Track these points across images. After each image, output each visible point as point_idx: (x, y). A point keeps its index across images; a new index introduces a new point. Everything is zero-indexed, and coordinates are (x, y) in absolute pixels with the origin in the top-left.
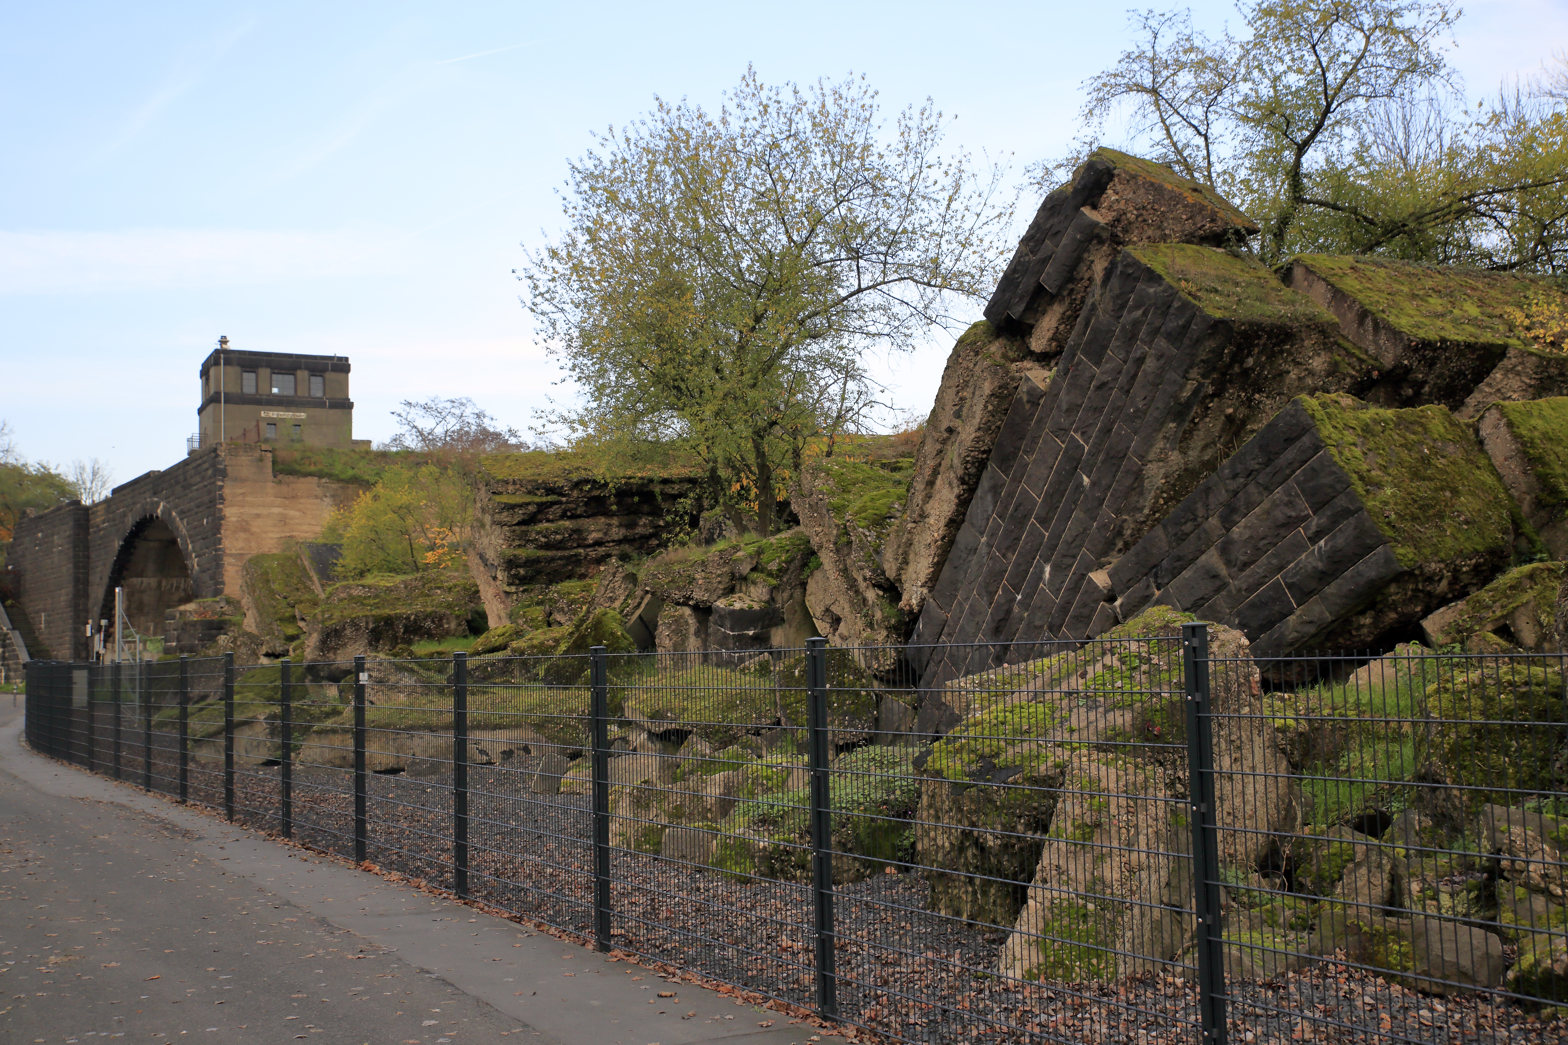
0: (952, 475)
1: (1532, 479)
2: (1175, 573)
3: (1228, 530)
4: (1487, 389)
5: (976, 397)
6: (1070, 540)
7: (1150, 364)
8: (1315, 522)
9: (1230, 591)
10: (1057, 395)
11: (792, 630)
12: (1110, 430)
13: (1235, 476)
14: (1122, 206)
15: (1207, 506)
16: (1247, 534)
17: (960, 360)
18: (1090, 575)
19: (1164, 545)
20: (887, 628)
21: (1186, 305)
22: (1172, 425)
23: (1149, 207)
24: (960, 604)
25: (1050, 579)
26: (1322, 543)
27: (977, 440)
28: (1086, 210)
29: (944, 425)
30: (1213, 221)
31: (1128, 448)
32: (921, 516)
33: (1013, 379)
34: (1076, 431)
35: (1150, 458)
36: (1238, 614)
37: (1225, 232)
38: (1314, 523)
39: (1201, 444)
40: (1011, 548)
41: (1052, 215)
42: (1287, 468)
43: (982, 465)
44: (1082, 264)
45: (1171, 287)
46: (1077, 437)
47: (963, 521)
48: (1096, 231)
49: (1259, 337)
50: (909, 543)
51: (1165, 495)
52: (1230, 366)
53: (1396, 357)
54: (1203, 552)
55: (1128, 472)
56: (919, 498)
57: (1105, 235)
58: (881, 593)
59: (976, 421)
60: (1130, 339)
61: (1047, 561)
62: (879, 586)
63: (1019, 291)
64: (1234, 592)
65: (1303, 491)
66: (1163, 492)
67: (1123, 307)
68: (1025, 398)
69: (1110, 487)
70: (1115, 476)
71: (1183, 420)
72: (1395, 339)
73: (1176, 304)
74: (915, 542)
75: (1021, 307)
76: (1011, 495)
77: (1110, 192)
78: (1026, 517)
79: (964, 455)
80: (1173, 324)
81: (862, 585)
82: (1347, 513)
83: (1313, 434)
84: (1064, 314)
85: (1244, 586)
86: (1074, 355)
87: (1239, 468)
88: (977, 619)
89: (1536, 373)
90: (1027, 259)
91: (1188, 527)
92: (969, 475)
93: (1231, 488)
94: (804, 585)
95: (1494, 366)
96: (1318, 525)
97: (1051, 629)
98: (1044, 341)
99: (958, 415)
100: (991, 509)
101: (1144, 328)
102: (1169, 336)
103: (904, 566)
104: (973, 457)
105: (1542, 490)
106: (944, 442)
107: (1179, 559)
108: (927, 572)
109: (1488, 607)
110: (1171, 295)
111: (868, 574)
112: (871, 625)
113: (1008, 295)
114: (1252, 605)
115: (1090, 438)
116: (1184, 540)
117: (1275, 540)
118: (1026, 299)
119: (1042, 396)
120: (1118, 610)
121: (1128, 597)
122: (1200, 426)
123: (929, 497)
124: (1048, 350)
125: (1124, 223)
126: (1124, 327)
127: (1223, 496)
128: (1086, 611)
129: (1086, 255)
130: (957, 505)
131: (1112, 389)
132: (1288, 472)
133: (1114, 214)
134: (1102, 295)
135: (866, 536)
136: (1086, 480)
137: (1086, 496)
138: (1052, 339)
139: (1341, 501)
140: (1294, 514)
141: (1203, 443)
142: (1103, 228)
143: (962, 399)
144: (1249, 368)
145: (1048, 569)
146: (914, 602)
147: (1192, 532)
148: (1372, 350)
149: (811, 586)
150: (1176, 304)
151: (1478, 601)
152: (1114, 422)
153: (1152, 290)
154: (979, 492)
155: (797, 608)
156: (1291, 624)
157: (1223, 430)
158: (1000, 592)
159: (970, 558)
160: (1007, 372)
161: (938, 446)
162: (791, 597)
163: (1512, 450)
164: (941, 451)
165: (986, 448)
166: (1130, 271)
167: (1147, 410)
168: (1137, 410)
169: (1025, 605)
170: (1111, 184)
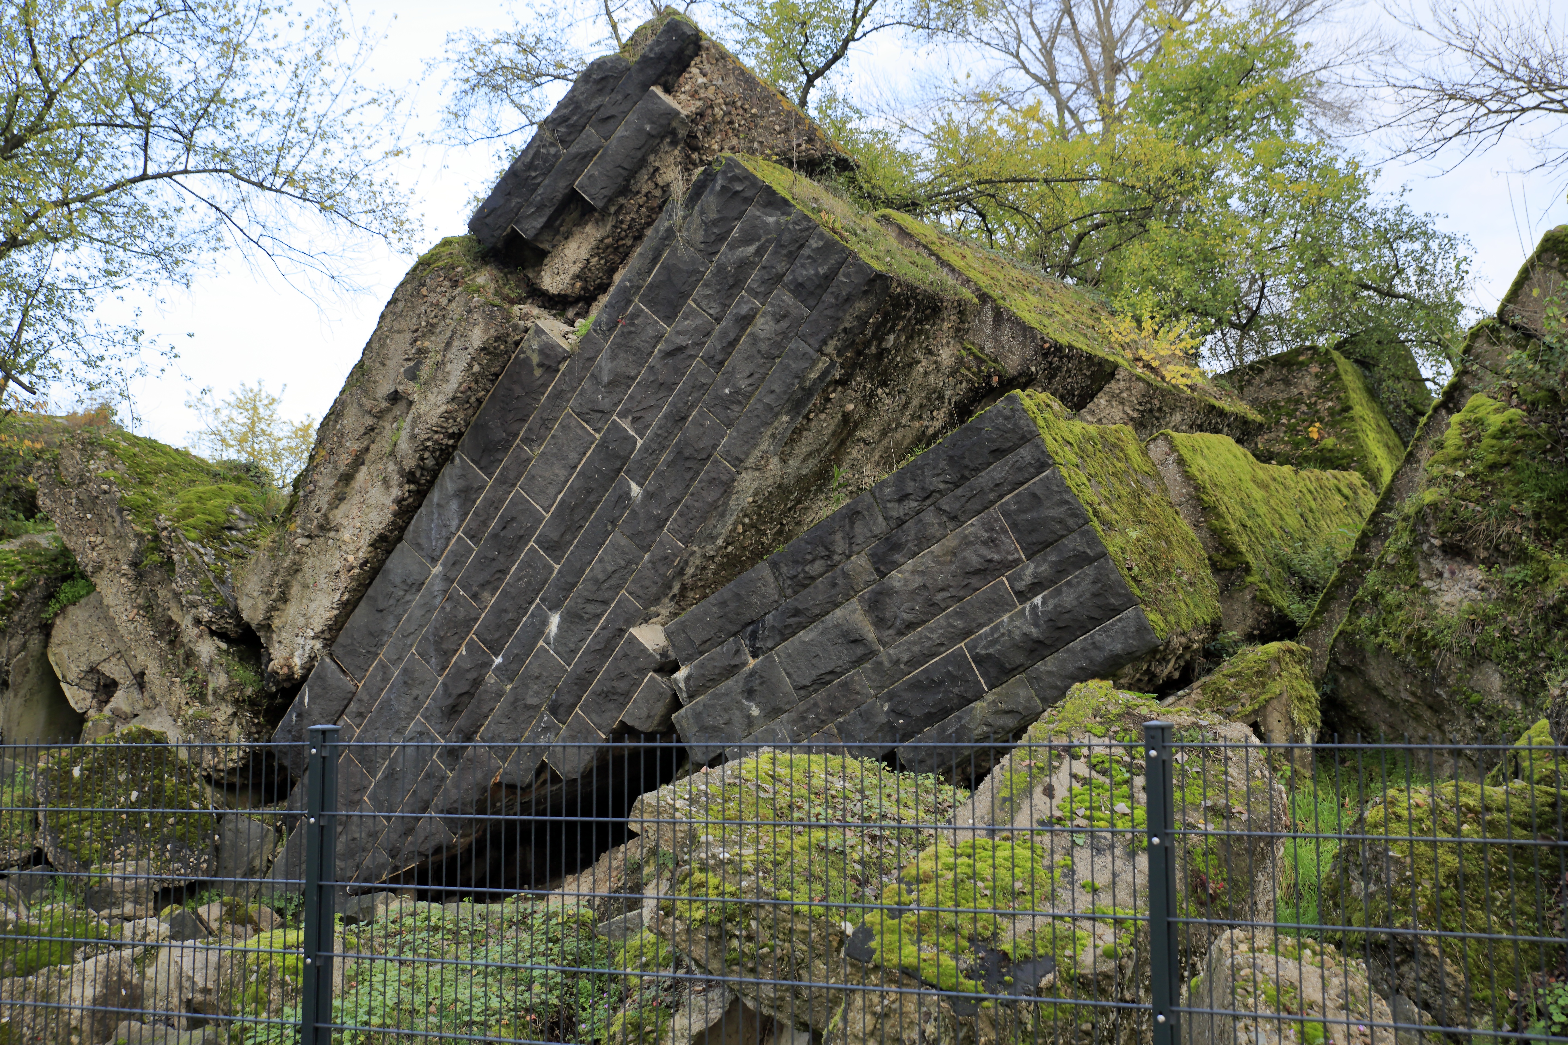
0: (391, 467)
1: (1205, 534)
2: (785, 633)
3: (883, 575)
4: (1089, 418)
5: (454, 350)
6: (601, 577)
7: (763, 326)
8: (1029, 571)
9: (880, 663)
10: (592, 359)
11: (19, 701)
12: (684, 419)
13: (903, 498)
14: (710, 93)
15: (850, 539)
16: (918, 581)
17: (424, 291)
18: (633, 630)
19: (771, 591)
20: (236, 702)
21: (830, 247)
22: (785, 418)
23: (739, 104)
24: (383, 667)
25: (558, 636)
26: (1038, 600)
27: (447, 416)
28: (658, 90)
29: (385, 388)
30: (810, 141)
31: (715, 447)
32: (321, 527)
33: (515, 327)
34: (621, 415)
35: (748, 464)
36: (890, 697)
37: (824, 158)
38: (1029, 571)
39: (806, 450)
40: (490, 585)
41: (600, 91)
42: (992, 490)
43: (444, 455)
44: (644, 171)
45: (806, 217)
46: (625, 424)
47: (400, 539)
48: (674, 124)
49: (908, 306)
50: (296, 569)
51: (747, 520)
52: (868, 344)
53: (1023, 359)
54: (837, 605)
55: (711, 481)
56: (322, 500)
57: (682, 133)
58: (224, 646)
59: (451, 387)
60: (731, 287)
61: (553, 608)
62: (222, 635)
63: (537, 197)
64: (887, 664)
65: (1014, 526)
66: (745, 515)
67: (721, 238)
68: (535, 359)
69: (678, 502)
70: (688, 486)
71: (799, 414)
72: (1025, 337)
73: (814, 243)
74: (305, 568)
75: (539, 222)
76: (493, 504)
77: (695, 71)
78: (522, 539)
79: (423, 436)
80: (806, 272)
81: (189, 631)
82: (1082, 560)
83: (1037, 446)
84: (601, 241)
85: (905, 657)
86: (629, 302)
87: (911, 486)
88: (415, 692)
89: (1140, 404)
90: (553, 150)
91: (817, 567)
92: (423, 468)
93: (895, 514)
94: (46, 630)
95: (1101, 389)
96: (1035, 575)
97: (554, 710)
98: (567, 279)
99: (412, 375)
100: (454, 523)
101: (755, 274)
102: (799, 289)
103: (280, 605)
104: (436, 442)
105: (1217, 550)
106: (380, 415)
107: (797, 613)
108: (328, 615)
109: (1235, 698)
110: (807, 229)
111: (206, 614)
112: (201, 697)
113: (515, 201)
114: (916, 685)
115: (647, 427)
116: (805, 586)
117: (961, 593)
118: (548, 212)
119: (564, 359)
120: (682, 685)
121: (702, 666)
122: (813, 424)
123: (340, 498)
124: (569, 292)
125: (709, 119)
126: (721, 269)
127: (880, 525)
128: (622, 686)
129: (652, 158)
130: (395, 515)
131: (693, 357)
132: (991, 496)
133: (699, 103)
134: (685, 218)
135: (200, 554)
136: (636, 490)
137: (633, 512)
138: (577, 277)
139: (1073, 543)
140: (996, 557)
141: (809, 449)
142: (682, 122)
143: (420, 351)
144: (886, 349)
145: (555, 620)
146: (297, 662)
147: (821, 575)
148: (990, 348)
149: (62, 630)
150: (814, 243)
151: (1218, 690)
152: (693, 406)
153: (771, 220)
154: (435, 496)
155: (30, 665)
156: (978, 713)
157: (834, 434)
158: (463, 650)
159: (408, 597)
160: (508, 318)
161: (369, 421)
162: (24, 646)
163: (1182, 495)
164: (372, 429)
165: (455, 429)
166: (739, 188)
167: (753, 393)
168: (737, 392)
169: (507, 672)
170: (697, 60)
